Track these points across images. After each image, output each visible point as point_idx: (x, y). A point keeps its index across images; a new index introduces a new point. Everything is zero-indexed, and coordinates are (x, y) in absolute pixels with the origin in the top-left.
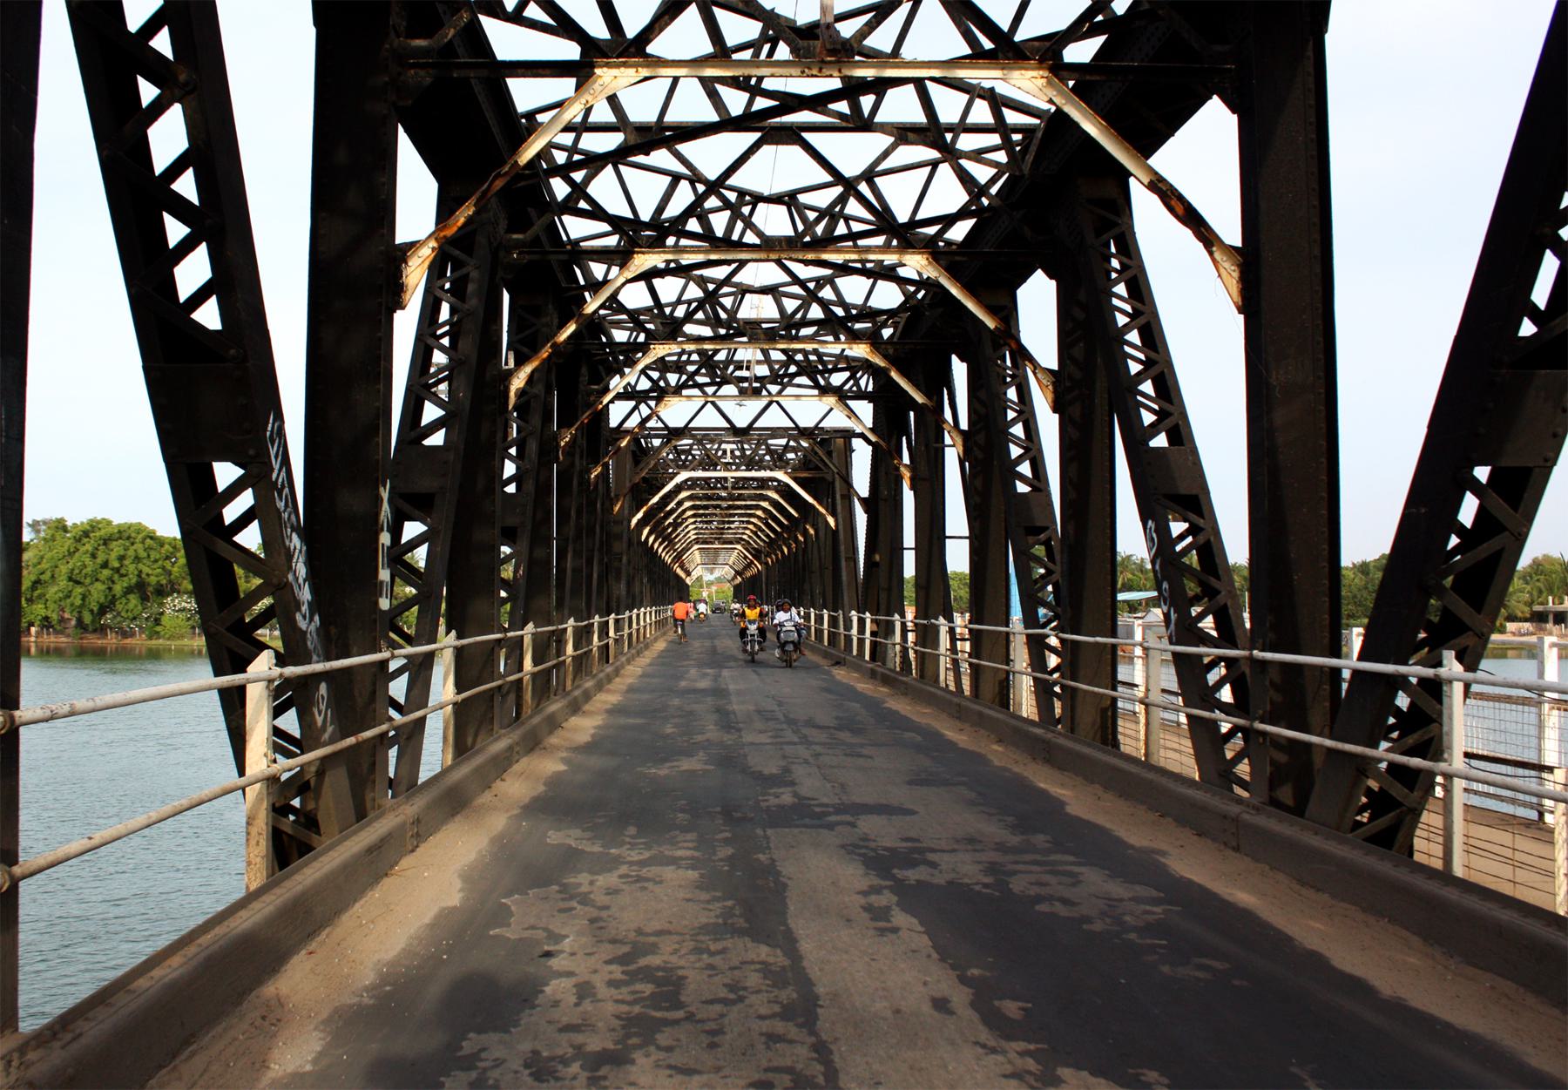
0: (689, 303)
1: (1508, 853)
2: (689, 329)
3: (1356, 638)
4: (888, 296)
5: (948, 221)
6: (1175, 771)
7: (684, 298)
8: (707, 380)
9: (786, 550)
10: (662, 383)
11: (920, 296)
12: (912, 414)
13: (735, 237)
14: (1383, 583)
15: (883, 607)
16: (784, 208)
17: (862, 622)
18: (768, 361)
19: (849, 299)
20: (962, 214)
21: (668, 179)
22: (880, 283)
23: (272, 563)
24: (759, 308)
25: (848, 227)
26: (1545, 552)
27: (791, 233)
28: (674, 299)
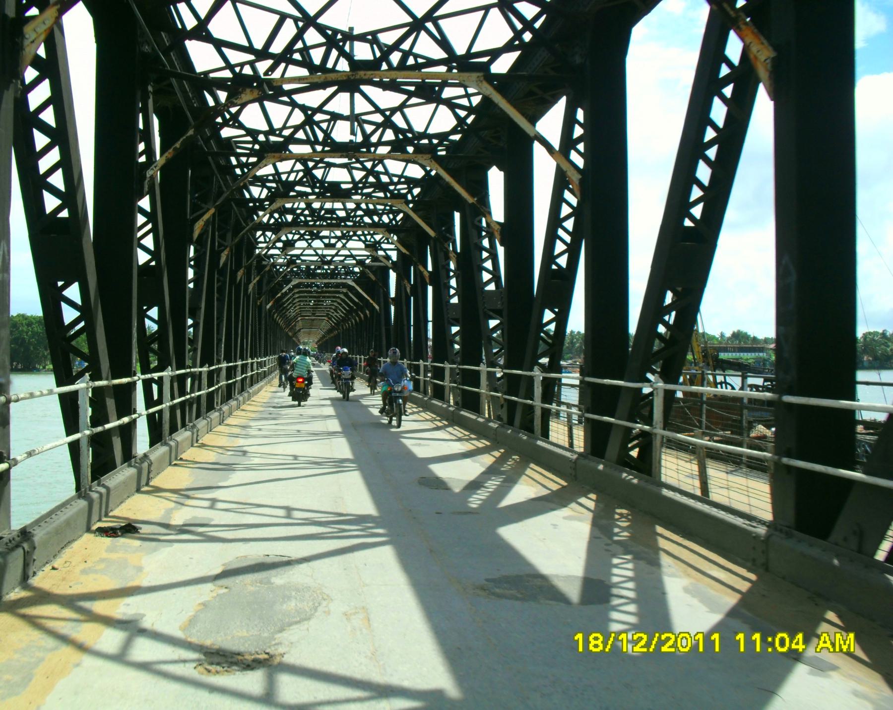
0: (298, 172)
1: (750, 490)
2: (295, 149)
3: (430, 360)
4: (444, 121)
5: (495, 54)
6: (555, 442)
7: (295, 169)
8: (309, 237)
9: (353, 321)
10: (280, 220)
11: (469, 121)
12: (457, 216)
13: (330, 65)
14: (70, 365)
15: (355, 353)
16: (368, 45)
17: (360, 359)
18: (345, 209)
19: (391, 171)
20: (508, 47)
21: (278, 17)
22: (410, 165)
23: (192, 342)
24: (342, 133)
25: (416, 60)
26: (739, 329)
27: (371, 58)
28: (289, 170)
